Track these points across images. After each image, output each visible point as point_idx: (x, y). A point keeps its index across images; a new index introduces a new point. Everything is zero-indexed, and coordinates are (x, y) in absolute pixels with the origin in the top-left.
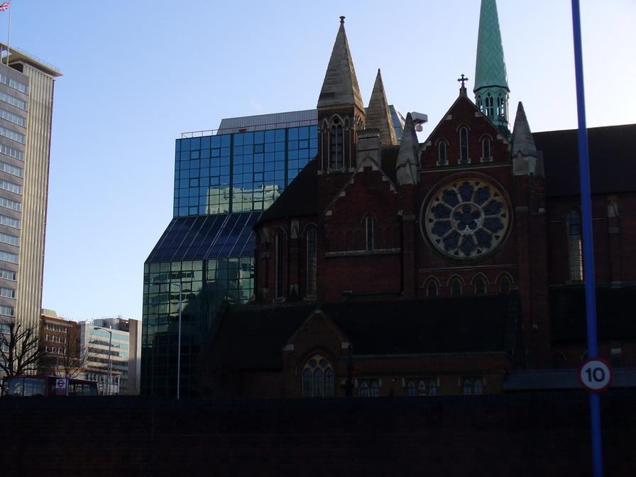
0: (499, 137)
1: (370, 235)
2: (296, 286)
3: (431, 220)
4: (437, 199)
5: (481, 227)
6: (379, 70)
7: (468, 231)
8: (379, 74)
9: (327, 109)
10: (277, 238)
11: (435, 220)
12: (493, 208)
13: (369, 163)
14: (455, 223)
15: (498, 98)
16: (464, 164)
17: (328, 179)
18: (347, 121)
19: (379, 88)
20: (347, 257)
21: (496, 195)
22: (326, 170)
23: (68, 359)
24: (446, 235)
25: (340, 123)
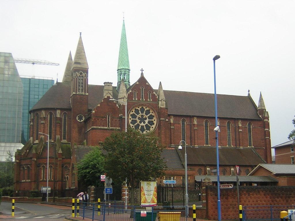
0: (154, 93)
1: (109, 122)
2: (59, 136)
3: (130, 119)
4: (133, 112)
5: (147, 123)
7: (142, 124)
8: (70, 53)
9: (78, 68)
10: (49, 116)
11: (132, 119)
13: (109, 95)
14: (138, 121)
15: (124, 73)
17: (78, 96)
18: (85, 74)
19: (261, 100)
20: (100, 129)
21: (152, 113)
22: (76, 93)
24: (145, 128)
25: (82, 75)
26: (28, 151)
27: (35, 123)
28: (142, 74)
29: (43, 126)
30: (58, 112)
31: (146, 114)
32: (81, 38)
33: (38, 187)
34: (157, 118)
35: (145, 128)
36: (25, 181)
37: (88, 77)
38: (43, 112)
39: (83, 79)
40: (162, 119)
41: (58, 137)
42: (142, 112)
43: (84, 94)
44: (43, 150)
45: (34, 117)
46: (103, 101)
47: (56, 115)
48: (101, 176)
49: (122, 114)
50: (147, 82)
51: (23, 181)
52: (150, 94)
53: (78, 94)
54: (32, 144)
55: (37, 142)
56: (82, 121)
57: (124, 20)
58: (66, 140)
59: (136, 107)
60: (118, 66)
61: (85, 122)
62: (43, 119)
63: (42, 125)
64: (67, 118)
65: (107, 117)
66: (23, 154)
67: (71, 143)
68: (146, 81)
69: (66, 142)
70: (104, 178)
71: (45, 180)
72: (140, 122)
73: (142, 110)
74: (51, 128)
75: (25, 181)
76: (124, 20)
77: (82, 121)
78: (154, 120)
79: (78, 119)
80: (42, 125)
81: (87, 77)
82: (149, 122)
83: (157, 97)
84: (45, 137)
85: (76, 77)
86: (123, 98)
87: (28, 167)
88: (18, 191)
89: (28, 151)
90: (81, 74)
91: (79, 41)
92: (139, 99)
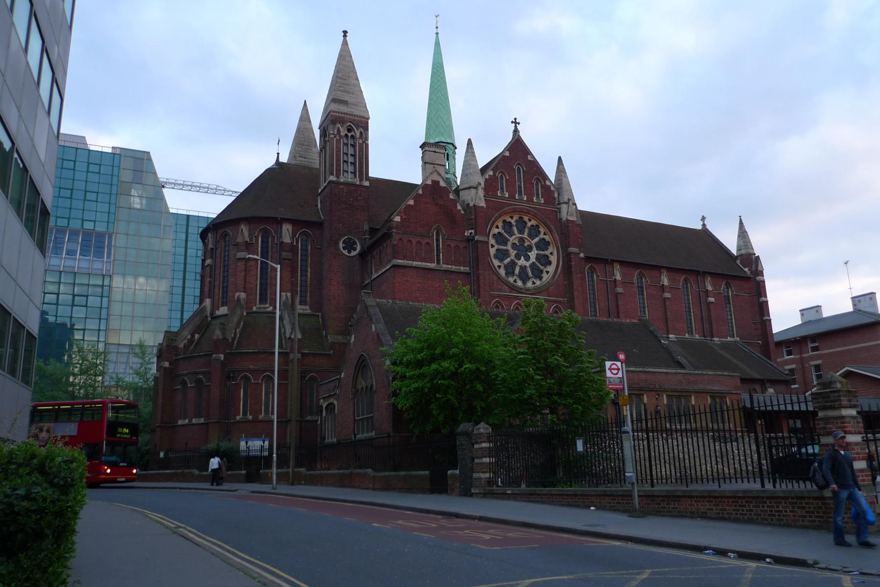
1: (438, 250)
2: (289, 294)
4: (497, 227)
7: (522, 262)
11: (496, 247)
12: (543, 245)
18: (361, 133)
19: (743, 234)
21: (545, 234)
24: (530, 274)
25: (353, 133)
26: (197, 336)
28: (516, 131)
29: (243, 267)
30: (287, 228)
31: (531, 236)
32: (345, 43)
35: (530, 274)
36: (187, 421)
38: (244, 229)
39: (355, 143)
40: (573, 249)
41: (286, 296)
42: (521, 232)
43: (358, 183)
45: (216, 242)
47: (281, 237)
51: (180, 422)
52: (537, 184)
53: (342, 180)
54: (209, 319)
55: (223, 310)
56: (354, 253)
57: (437, 33)
58: (307, 307)
59: (505, 213)
61: (362, 255)
62: (244, 248)
63: (241, 265)
64: (309, 247)
66: (182, 346)
67: (322, 315)
68: (526, 151)
69: (309, 311)
70: (620, 375)
71: (250, 417)
72: (518, 257)
73: (521, 224)
74: (267, 273)
75: (187, 421)
76: (437, 33)
77: (354, 253)
78: (551, 253)
79: (344, 248)
80: (239, 264)
81: (367, 139)
82: (538, 257)
85: (338, 137)
86: (476, 188)
87: (199, 382)
88: (166, 454)
89: (197, 336)
90: (349, 130)
91: (342, 50)
92: (512, 196)
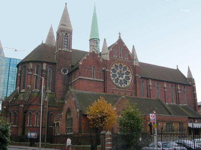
6: (105, 39)
7: (121, 78)
8: (189, 67)
16: (121, 58)
19: (189, 72)
23: (64, 57)
24: (123, 82)
25: (67, 35)
26: (15, 99)
27: (22, 74)
28: (120, 36)
30: (45, 65)
32: (66, 7)
33: (23, 132)
34: (132, 74)
37: (72, 37)
38: (31, 64)
44: (29, 98)
45: (22, 68)
46: (89, 55)
48: (151, 115)
49: (105, 68)
50: (124, 44)
56: (66, 74)
59: (116, 63)
60: (91, 36)
61: (68, 74)
62: (31, 71)
63: (29, 76)
65: (92, 69)
66: (10, 101)
71: (31, 126)
72: (119, 77)
77: (66, 74)
78: (130, 76)
79: (63, 72)
83: (132, 57)
84: (31, 86)
87: (15, 113)
89: (15, 99)
90: (66, 34)
